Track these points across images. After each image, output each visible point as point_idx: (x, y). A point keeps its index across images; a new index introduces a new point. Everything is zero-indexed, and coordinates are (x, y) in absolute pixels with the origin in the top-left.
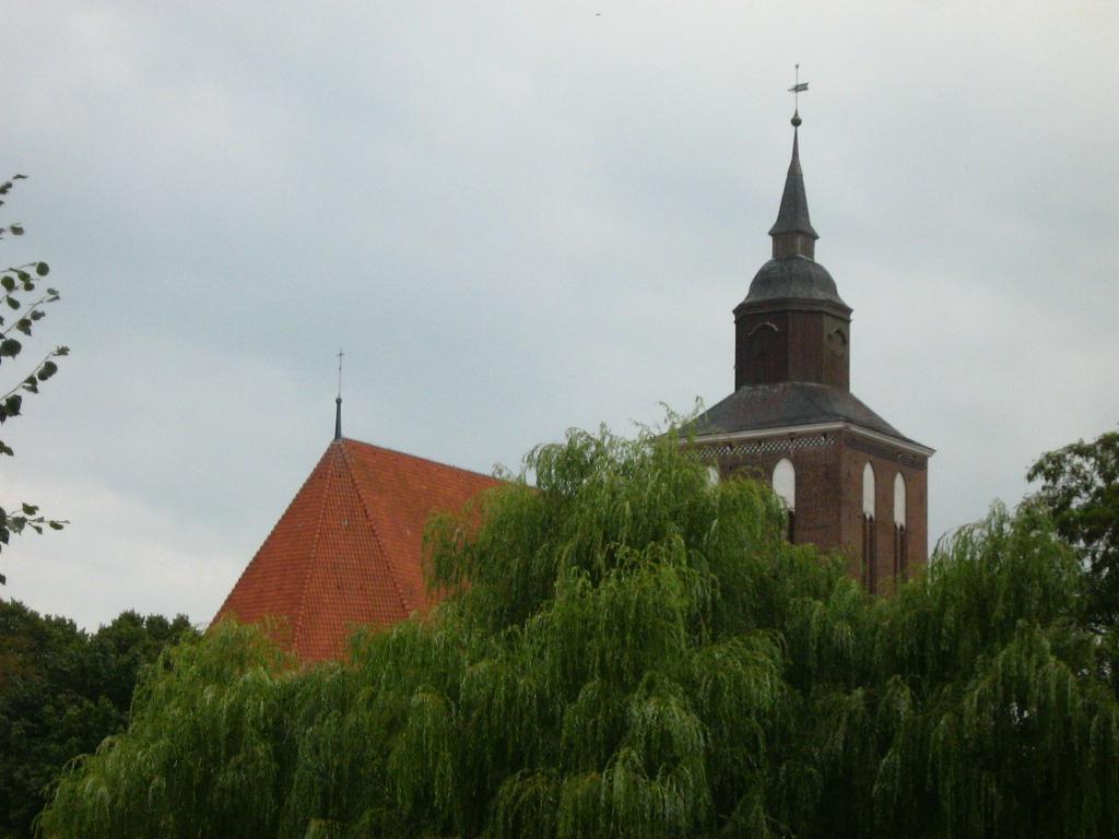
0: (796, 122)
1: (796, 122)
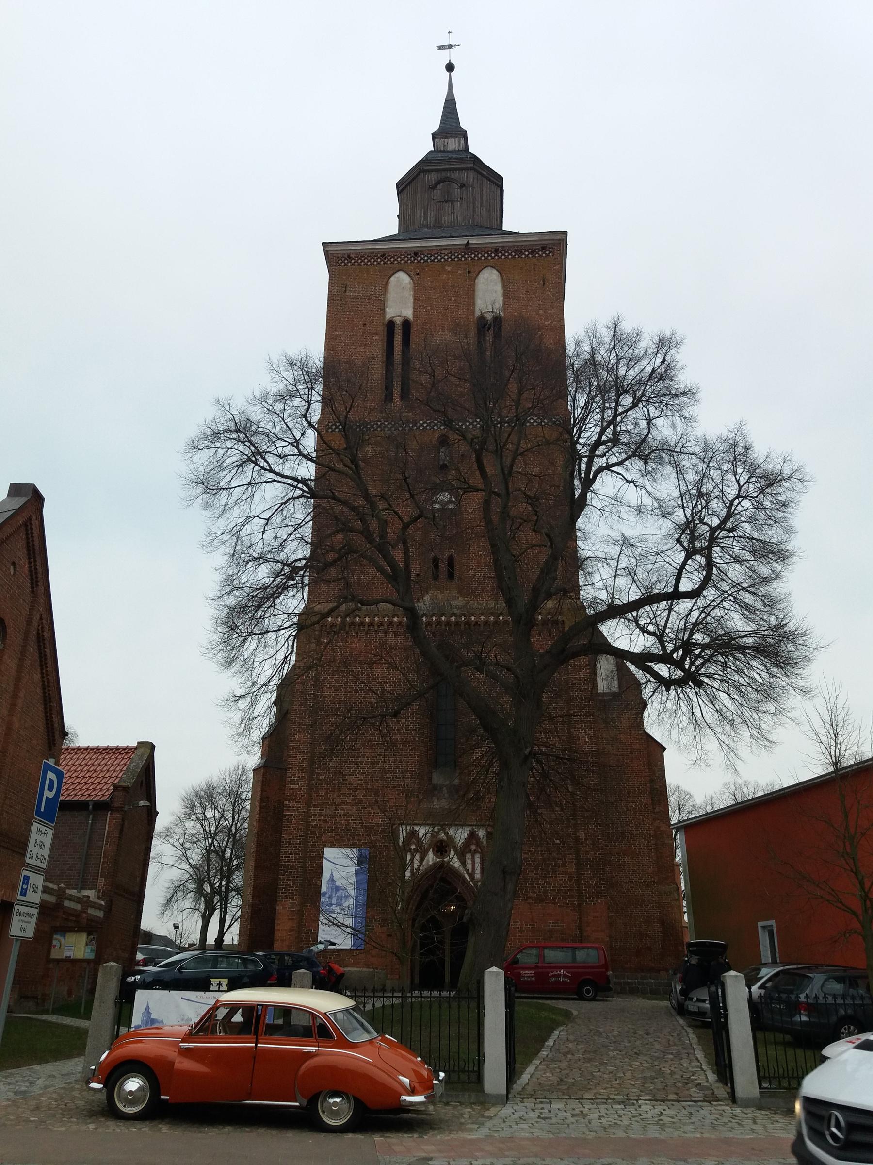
0: (450, 67)
1: (450, 67)
